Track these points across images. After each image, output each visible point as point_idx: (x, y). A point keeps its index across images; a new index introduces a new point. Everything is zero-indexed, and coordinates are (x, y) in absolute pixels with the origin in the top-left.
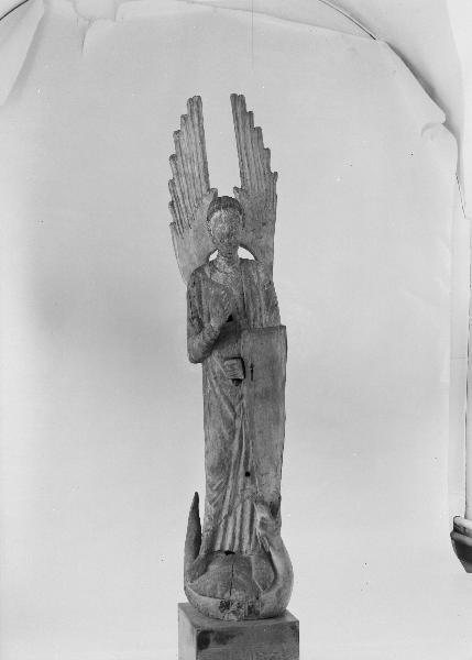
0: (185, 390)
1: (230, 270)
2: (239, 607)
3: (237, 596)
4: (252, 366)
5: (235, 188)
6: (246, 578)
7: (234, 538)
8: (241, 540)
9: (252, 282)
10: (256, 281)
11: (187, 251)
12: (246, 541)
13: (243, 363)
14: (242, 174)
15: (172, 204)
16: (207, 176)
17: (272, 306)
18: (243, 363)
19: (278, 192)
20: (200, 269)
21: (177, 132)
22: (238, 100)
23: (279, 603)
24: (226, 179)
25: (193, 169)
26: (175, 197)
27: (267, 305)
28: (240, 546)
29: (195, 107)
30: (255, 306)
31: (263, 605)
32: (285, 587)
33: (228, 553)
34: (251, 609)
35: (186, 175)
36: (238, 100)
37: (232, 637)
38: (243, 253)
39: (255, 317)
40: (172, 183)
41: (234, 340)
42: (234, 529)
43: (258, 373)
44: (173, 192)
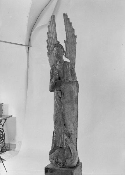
0: (49, 98)
1: (60, 65)
2: (60, 164)
3: (60, 160)
4: (64, 93)
5: (64, 41)
6: (62, 155)
7: (61, 143)
8: (63, 144)
9: (66, 68)
10: (68, 68)
11: (51, 60)
12: (64, 144)
13: (61, 92)
14: (66, 36)
15: (47, 46)
16: (56, 38)
17: (73, 75)
18: (61, 92)
19: (77, 41)
20: (54, 65)
21: (49, 26)
22: (65, 15)
23: (72, 164)
24: (62, 38)
25: (53, 36)
26: (48, 44)
27: (71, 75)
28: (63, 146)
29: (53, 18)
30: (67, 75)
31: (66, 164)
32: (73, 159)
33: (60, 147)
34: (63, 165)
35: (51, 38)
36: (65, 15)
37: (54, 171)
38: (65, 59)
39: (67, 78)
40: (47, 40)
41: (74, 87)
42: (61, 141)
43: (66, 95)
44: (48, 43)
